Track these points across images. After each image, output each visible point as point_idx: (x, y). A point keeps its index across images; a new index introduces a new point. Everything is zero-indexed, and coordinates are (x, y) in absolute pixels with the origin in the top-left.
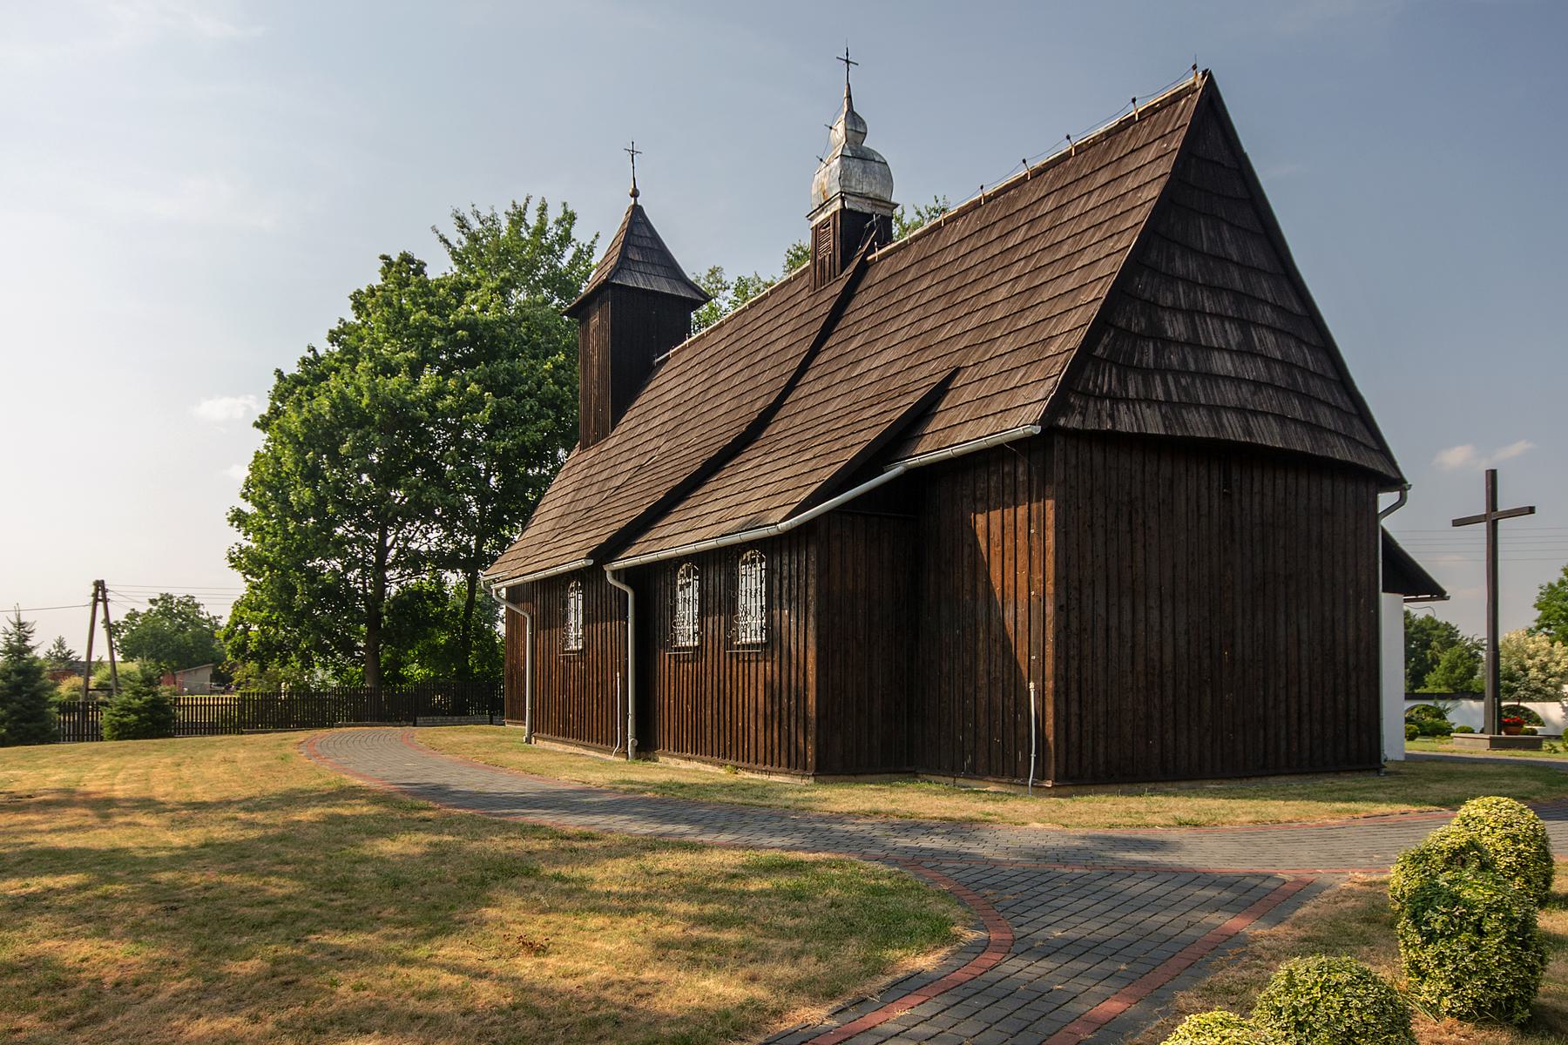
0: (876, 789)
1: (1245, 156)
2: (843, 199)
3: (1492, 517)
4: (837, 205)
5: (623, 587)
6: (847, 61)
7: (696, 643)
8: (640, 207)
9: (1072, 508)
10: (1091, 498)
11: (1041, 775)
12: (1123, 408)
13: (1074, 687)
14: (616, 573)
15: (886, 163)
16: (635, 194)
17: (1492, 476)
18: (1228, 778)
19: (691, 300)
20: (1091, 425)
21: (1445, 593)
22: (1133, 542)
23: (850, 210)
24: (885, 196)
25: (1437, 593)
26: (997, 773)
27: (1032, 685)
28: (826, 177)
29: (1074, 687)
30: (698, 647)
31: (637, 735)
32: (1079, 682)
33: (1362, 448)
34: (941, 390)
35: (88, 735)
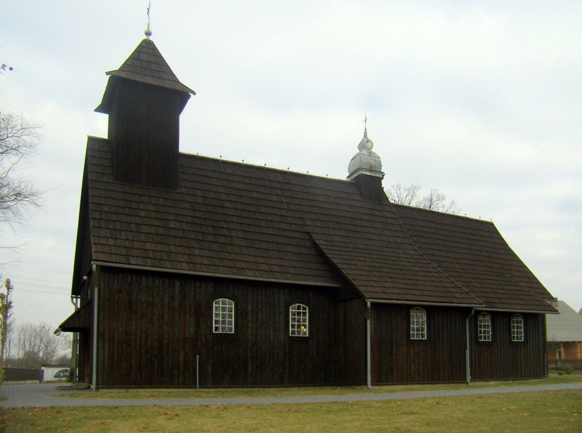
31: (471, 375)
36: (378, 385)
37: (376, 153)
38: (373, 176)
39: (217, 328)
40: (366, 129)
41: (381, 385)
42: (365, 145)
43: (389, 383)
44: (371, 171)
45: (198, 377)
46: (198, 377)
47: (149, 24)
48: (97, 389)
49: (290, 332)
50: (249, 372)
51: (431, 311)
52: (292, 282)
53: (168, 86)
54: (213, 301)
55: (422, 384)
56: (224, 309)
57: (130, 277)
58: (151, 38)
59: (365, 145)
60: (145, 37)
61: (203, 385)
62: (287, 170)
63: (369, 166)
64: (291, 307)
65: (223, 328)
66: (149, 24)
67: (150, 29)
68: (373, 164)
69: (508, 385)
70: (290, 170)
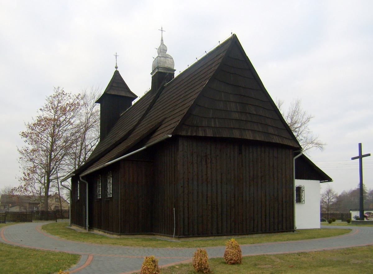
0: (116, 238)
1: (247, 57)
2: (158, 69)
3: (361, 157)
5: (85, 182)
6: (162, 30)
7: (111, 196)
8: (118, 71)
9: (186, 158)
10: (192, 155)
11: (176, 234)
12: (200, 129)
13: (186, 209)
14: (83, 177)
15: (172, 58)
16: (116, 68)
17: (360, 145)
18: (241, 235)
19: (132, 98)
20: (189, 134)
21: (332, 179)
22: (207, 167)
23: (159, 72)
24: (171, 67)
25: (330, 180)
26: (231, 232)
27: (174, 209)
28: (116, 66)
29: (186, 209)
30: (112, 197)
32: (188, 208)
33: (285, 139)
34: (160, 124)
35: (7, 220)
40: (162, 37)
42: (162, 50)
47: (116, 63)
59: (162, 50)
60: (115, 70)
66: (116, 63)
67: (117, 66)
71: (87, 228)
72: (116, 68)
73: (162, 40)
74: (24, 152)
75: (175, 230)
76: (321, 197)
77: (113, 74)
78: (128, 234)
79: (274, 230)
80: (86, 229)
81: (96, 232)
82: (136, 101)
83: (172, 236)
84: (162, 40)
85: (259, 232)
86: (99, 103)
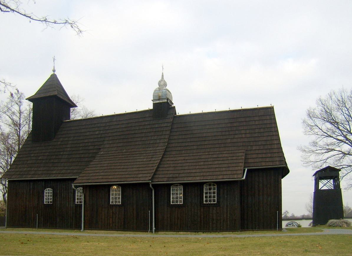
1: (51, 76)
4: (166, 101)
8: (56, 75)
16: (54, 71)
31: (155, 227)
36: (90, 230)
37: (156, 88)
38: (160, 103)
39: (206, 201)
41: (92, 230)
42: (162, 84)
43: (141, 231)
44: (159, 100)
45: (149, 225)
46: (149, 225)
48: (84, 229)
49: (171, 202)
50: (58, 222)
51: (124, 187)
52: (48, 178)
53: (52, 94)
54: (45, 189)
55: (117, 231)
56: (49, 193)
57: (17, 183)
58: (56, 73)
59: (162, 84)
60: (52, 73)
61: (39, 227)
62: (136, 111)
63: (158, 97)
64: (45, 190)
65: (116, 202)
66: (54, 67)
67: (55, 69)
68: (160, 95)
69: (156, 235)
70: (116, 114)
71: (153, 230)
72: (54, 71)
73: (163, 76)
74: (314, 149)
75: (150, 226)
76: (311, 205)
77: (49, 76)
78: (111, 230)
79: (31, 227)
80: (152, 232)
81: (39, 229)
82: (176, 115)
83: (276, 229)
84: (163, 76)
85: (73, 229)
86: (153, 108)
